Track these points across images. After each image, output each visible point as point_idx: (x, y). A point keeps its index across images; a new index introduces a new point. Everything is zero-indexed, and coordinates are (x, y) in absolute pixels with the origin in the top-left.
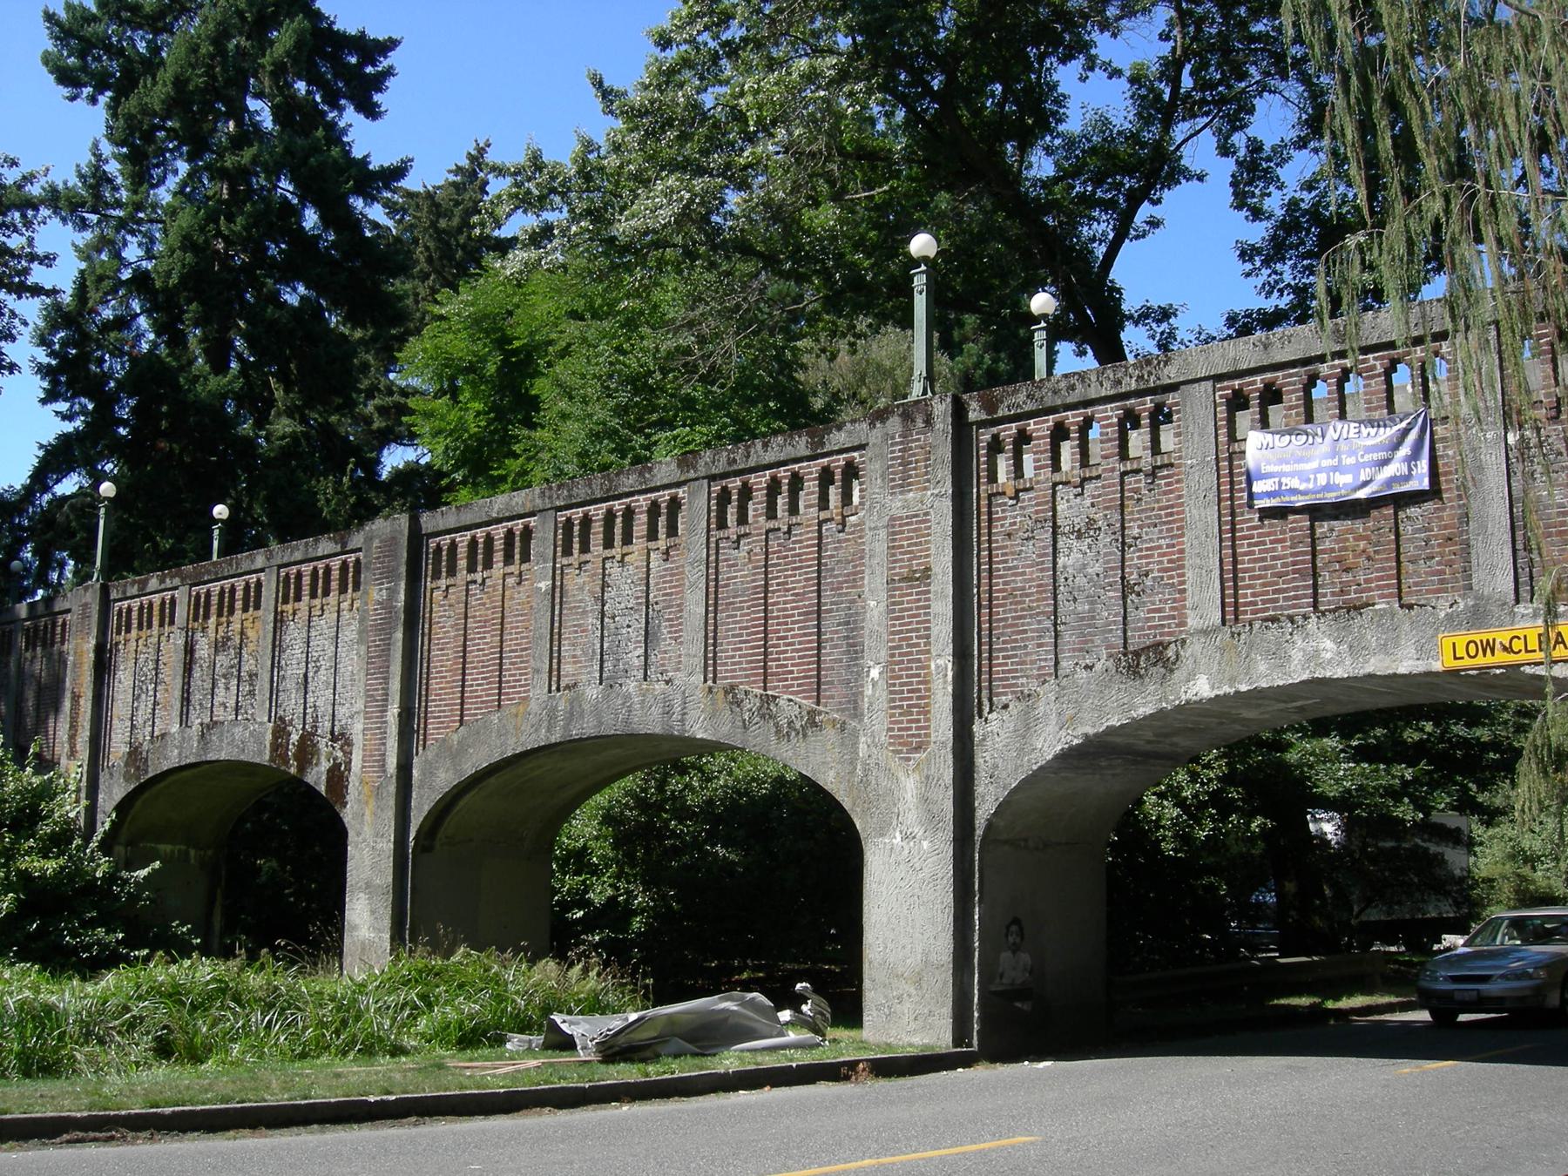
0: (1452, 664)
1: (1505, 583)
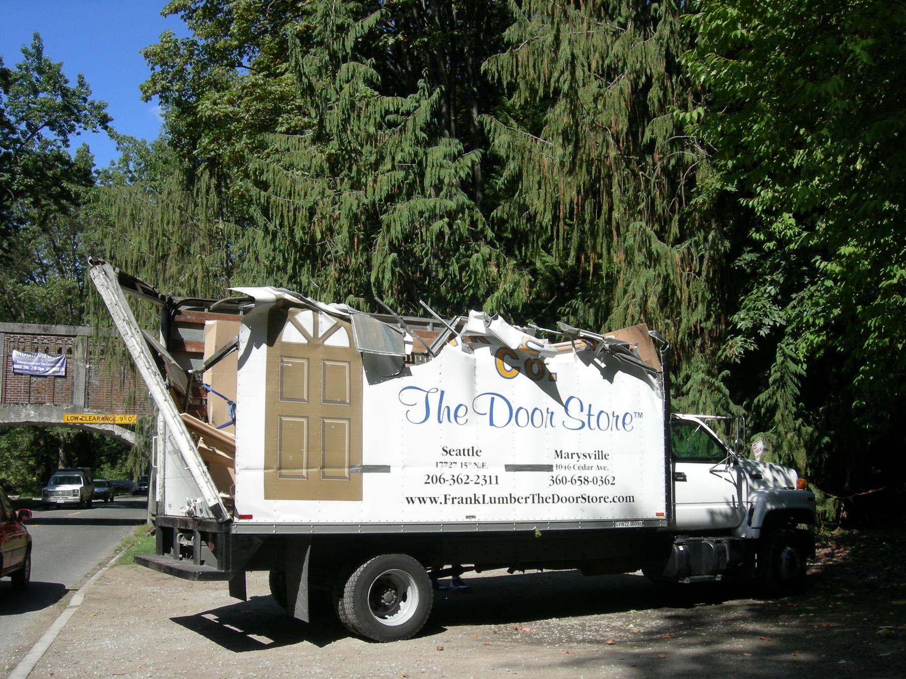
0: (66, 421)
1: (82, 403)
